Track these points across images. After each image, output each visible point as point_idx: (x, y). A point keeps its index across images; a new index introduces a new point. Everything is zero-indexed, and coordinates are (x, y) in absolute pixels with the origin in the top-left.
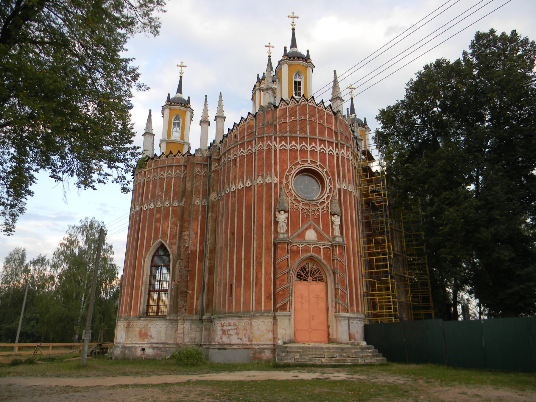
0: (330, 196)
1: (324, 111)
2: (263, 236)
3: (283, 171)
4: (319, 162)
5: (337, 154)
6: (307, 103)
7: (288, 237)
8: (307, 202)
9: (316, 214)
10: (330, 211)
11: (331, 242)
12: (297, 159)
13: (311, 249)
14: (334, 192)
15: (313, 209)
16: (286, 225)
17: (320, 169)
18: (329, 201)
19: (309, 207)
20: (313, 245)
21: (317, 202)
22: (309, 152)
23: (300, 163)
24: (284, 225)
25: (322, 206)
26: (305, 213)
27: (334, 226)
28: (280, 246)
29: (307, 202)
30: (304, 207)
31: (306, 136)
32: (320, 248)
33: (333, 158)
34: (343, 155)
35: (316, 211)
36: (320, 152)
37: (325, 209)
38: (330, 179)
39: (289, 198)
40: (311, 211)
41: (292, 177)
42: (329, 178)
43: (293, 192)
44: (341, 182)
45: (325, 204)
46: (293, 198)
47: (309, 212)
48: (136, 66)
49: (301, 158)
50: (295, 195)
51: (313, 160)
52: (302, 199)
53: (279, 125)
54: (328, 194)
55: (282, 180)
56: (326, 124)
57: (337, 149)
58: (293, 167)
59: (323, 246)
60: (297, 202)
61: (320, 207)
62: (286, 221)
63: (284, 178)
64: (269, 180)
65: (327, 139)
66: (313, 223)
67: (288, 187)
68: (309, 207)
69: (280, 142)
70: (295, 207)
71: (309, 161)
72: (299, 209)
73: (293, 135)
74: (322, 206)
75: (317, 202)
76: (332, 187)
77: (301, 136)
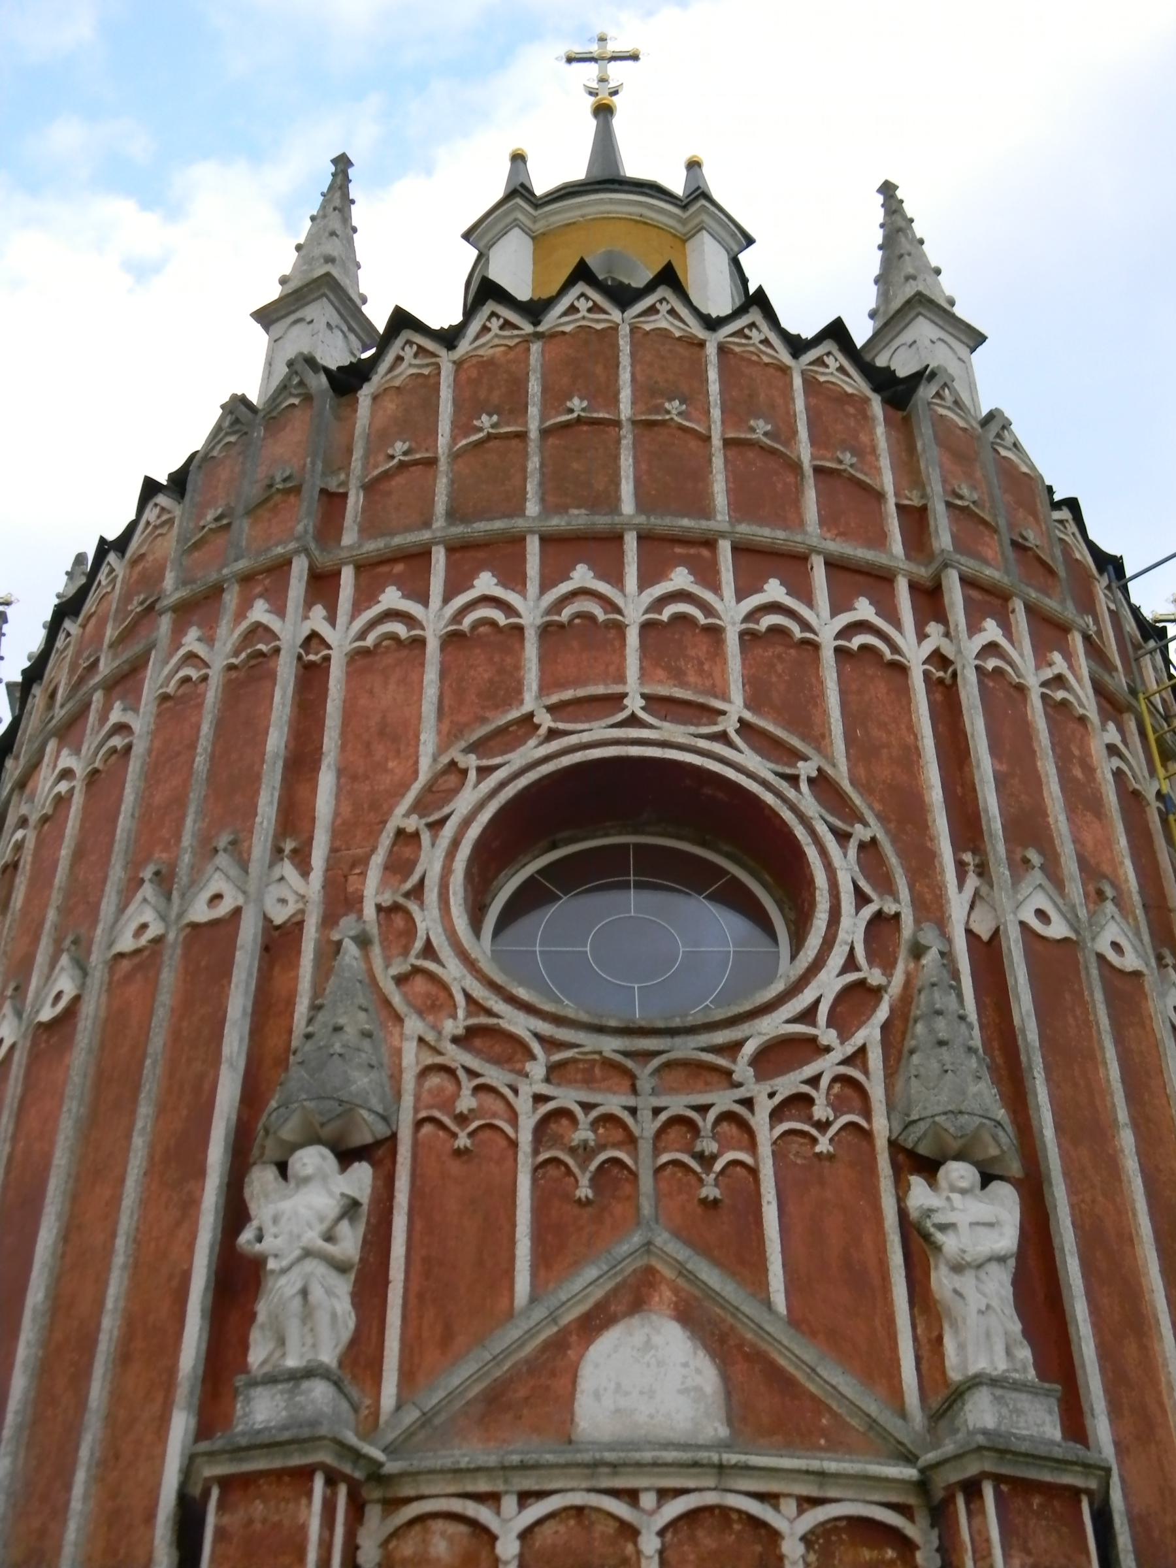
0: (876, 993)
1: (784, 370)
2: (84, 1453)
3: (375, 806)
4: (735, 708)
5: (938, 658)
6: (616, 315)
7: (370, 1425)
8: (610, 1045)
9: (707, 1161)
10: (881, 1126)
11: (909, 1458)
12: (515, 694)
13: (650, 1544)
14: (918, 951)
15: (677, 1104)
16: (343, 1287)
17: (751, 760)
18: (869, 1033)
19: (634, 1091)
20: (665, 1495)
21: (721, 1037)
22: (633, 637)
23: (545, 721)
24: (317, 1293)
25: (789, 1084)
26: (584, 1152)
27: (942, 1281)
28: (233, 1520)
29: (610, 1045)
30: (567, 1097)
31: (602, 521)
32: (774, 1536)
33: (904, 691)
34: (991, 664)
35: (706, 1123)
36: (749, 638)
37: (821, 1111)
38: (869, 848)
39: (414, 1025)
40: (646, 1127)
41: (455, 843)
42: (861, 833)
43: (452, 971)
44: (1001, 871)
45: (827, 1066)
46: (451, 1027)
47: (631, 1141)
48: (620, 1108)
49: (544, 688)
50: (545, 1028)
51: (679, 693)
52: (558, 1020)
53: (370, 488)
54: (851, 964)
55: (353, 884)
56: (805, 452)
57: (934, 629)
58: (471, 762)
59: (808, 1502)
60: (497, 1061)
61: (759, 1091)
62: (349, 1242)
63: (378, 860)
64: (218, 897)
65: (814, 541)
66: (679, 1251)
67: (410, 930)
68: (634, 1091)
69: (366, 596)
70: (466, 1102)
71: (634, 704)
72: (513, 1117)
73: (482, 527)
74: (789, 1084)
75: (721, 1037)
76: (902, 905)
77: (557, 523)
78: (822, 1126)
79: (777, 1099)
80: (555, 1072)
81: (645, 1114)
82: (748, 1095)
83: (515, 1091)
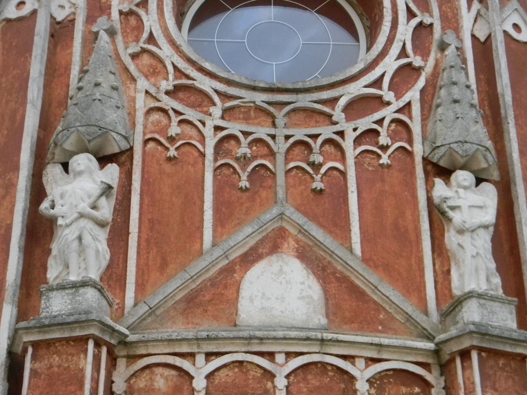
37: (383, 140)
78: (385, 148)
79: (359, 132)
80: (227, 113)
81: (280, 139)
82: (341, 129)
83: (204, 124)
